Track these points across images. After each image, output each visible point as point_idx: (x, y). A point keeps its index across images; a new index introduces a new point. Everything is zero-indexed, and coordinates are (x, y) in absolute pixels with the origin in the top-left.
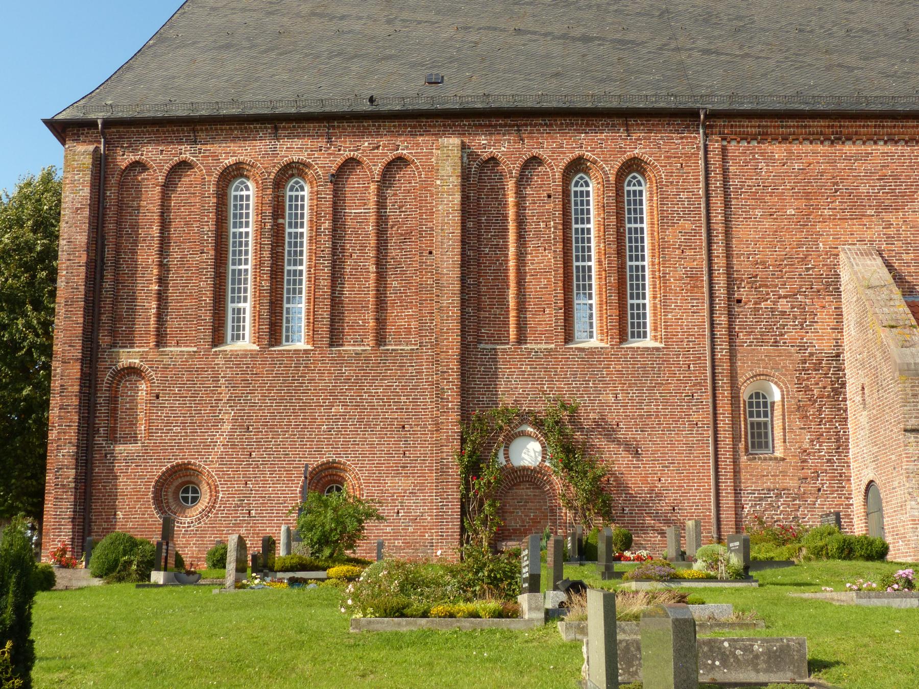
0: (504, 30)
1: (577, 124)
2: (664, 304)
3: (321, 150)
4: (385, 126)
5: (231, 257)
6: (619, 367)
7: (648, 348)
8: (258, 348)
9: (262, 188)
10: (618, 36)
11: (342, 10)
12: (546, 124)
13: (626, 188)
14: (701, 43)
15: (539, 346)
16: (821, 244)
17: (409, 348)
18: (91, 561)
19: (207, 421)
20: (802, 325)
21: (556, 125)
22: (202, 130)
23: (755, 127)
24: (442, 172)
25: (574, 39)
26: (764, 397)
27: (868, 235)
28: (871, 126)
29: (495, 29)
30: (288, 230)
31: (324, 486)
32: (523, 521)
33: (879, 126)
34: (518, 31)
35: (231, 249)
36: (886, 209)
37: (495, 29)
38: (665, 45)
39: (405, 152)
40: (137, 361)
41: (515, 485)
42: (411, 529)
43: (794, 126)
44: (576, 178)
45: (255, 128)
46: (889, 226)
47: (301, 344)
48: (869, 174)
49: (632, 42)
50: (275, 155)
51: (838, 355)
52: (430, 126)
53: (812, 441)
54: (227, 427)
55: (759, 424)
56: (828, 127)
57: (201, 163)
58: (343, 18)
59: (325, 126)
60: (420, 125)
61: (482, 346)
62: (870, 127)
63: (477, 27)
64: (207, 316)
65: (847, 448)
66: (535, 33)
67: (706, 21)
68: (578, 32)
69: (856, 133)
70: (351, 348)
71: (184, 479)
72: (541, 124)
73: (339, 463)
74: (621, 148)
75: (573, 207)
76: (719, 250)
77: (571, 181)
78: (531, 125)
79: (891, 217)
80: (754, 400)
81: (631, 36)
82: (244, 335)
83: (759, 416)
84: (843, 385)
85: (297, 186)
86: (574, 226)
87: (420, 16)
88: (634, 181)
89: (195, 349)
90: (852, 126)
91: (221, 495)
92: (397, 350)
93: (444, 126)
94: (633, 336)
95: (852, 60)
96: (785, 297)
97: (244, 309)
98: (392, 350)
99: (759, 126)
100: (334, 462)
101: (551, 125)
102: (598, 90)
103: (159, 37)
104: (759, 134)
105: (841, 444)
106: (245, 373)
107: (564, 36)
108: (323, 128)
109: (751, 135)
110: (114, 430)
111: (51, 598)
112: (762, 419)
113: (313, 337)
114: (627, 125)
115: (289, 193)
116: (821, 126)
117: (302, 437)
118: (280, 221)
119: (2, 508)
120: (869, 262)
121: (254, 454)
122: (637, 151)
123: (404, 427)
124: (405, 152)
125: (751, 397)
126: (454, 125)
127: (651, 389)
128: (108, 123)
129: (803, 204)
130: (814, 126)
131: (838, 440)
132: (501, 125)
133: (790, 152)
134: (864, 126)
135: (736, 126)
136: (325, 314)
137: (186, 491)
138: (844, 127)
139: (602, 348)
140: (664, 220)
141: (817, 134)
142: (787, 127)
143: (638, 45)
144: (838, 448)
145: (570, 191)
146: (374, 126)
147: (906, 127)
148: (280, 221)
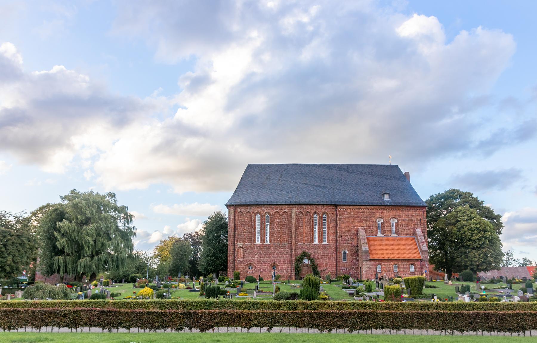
10: (323, 185)
11: (273, 178)
13: (323, 217)
14: (338, 187)
18: (437, 286)
25: (315, 186)
29: (301, 183)
36: (366, 221)
37: (301, 183)
46: (367, 224)
47: (268, 243)
49: (326, 187)
51: (357, 246)
54: (257, 257)
55: (344, 257)
58: (273, 179)
66: (308, 184)
67: (339, 181)
68: (316, 184)
81: (325, 185)
84: (358, 251)
86: (314, 223)
102: (318, 200)
107: (313, 185)
108: (272, 206)
128: (236, 205)
137: (250, 267)
143: (327, 188)
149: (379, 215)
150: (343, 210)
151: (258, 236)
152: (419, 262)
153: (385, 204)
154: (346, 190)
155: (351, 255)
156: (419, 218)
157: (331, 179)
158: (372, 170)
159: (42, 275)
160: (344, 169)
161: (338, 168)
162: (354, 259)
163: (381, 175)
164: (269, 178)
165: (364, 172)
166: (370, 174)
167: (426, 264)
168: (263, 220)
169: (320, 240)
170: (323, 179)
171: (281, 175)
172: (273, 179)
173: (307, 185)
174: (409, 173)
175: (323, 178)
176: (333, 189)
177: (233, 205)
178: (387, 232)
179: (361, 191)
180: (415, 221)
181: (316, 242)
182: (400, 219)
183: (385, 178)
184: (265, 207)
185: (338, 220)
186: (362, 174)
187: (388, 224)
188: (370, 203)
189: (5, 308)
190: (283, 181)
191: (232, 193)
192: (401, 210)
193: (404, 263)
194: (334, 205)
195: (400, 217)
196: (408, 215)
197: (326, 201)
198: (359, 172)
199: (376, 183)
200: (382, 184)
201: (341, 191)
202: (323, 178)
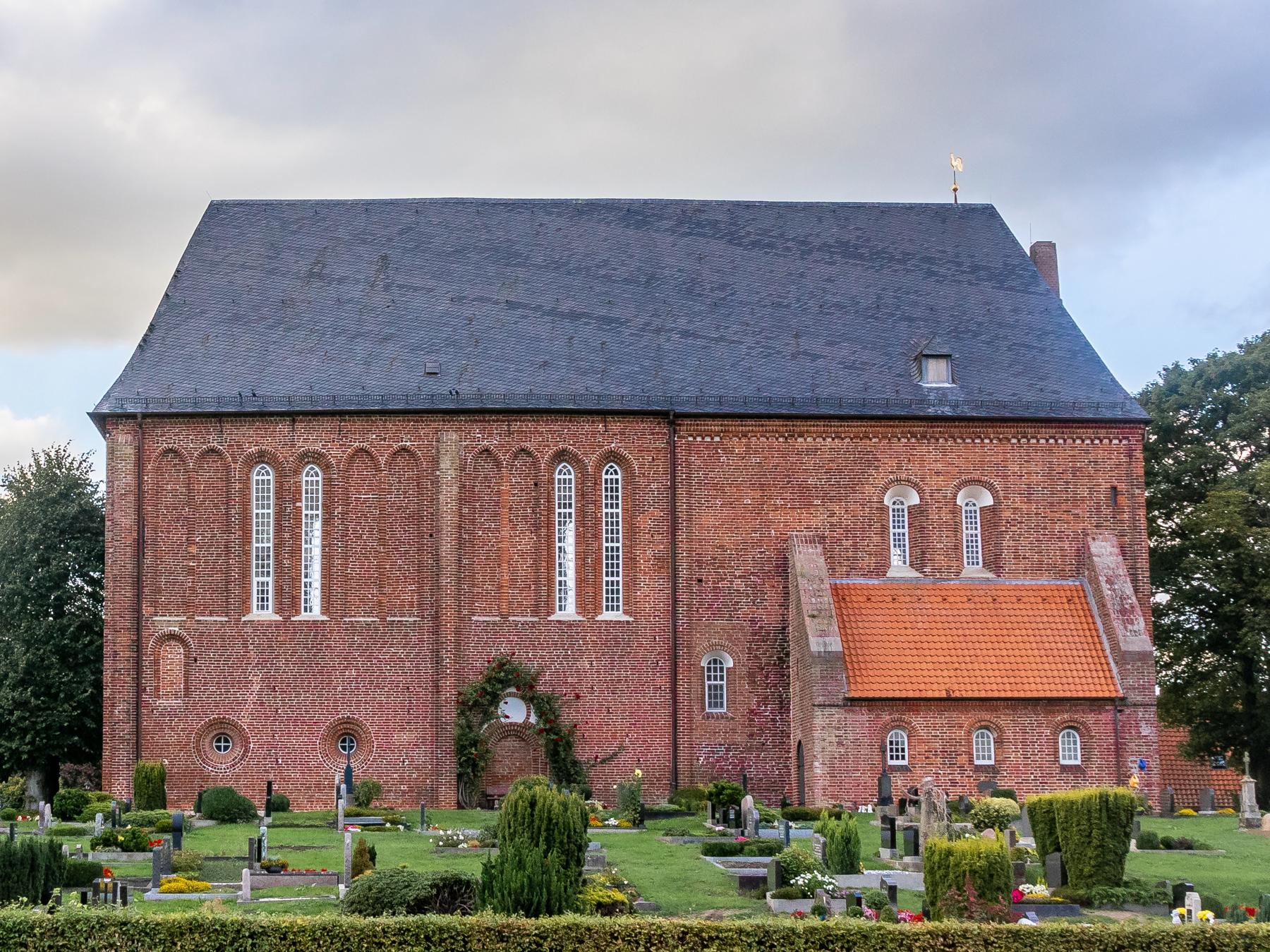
0: (497, 303)
1: (561, 420)
3: (334, 441)
4: (390, 420)
5: (254, 536)
6: (594, 638)
7: (620, 621)
8: (281, 619)
10: (603, 312)
11: (340, 272)
12: (533, 420)
14: (682, 322)
15: (525, 619)
16: (773, 532)
17: (412, 619)
18: (1202, 840)
19: (239, 682)
20: (754, 603)
21: (543, 421)
22: (227, 421)
23: (718, 426)
24: (442, 466)
25: (563, 315)
26: (721, 663)
27: (813, 523)
28: (820, 426)
30: (304, 512)
31: (339, 737)
32: (510, 769)
33: (827, 426)
34: (511, 305)
35: (255, 528)
38: (647, 324)
39: (408, 444)
40: (177, 629)
41: (503, 738)
42: (414, 776)
43: (752, 425)
44: (560, 467)
45: (275, 420)
47: (316, 613)
48: (818, 468)
49: (616, 320)
50: (293, 446)
51: (784, 629)
52: (431, 421)
53: (758, 703)
54: (256, 687)
55: (716, 686)
56: (783, 426)
57: (228, 452)
59: (337, 420)
60: (422, 420)
61: (474, 618)
62: (820, 426)
63: (471, 297)
65: (788, 710)
66: (525, 306)
67: (690, 291)
68: (565, 307)
69: (807, 431)
70: (362, 619)
71: (222, 731)
72: (529, 420)
73: (353, 718)
74: (599, 442)
75: (557, 493)
77: (554, 470)
78: (520, 421)
80: (712, 666)
81: (616, 313)
82: (267, 605)
83: (715, 679)
84: (788, 655)
85: (312, 472)
87: (417, 282)
88: (612, 470)
89: (226, 619)
90: (803, 426)
91: (252, 746)
92: (402, 621)
93: (444, 421)
94: (607, 609)
95: (817, 346)
96: (740, 577)
97: (267, 583)
98: (398, 621)
99: (721, 425)
100: (348, 717)
101: (538, 421)
104: (722, 432)
105: (783, 707)
106: (270, 640)
107: (552, 312)
108: (337, 422)
109: (715, 432)
110: (157, 689)
112: (719, 682)
113: (326, 610)
114: (605, 422)
115: (305, 479)
116: (776, 426)
117: (321, 696)
118: (298, 504)
120: (811, 550)
121: (280, 711)
122: (613, 445)
123: (408, 688)
124: (408, 444)
125: (709, 663)
126: (452, 420)
127: (621, 656)
128: (145, 416)
129: (758, 494)
130: (769, 426)
131: (781, 702)
132: (494, 421)
133: (748, 446)
134: (814, 426)
135: (701, 425)
138: (796, 426)
139: (579, 621)
141: (773, 432)
142: (745, 426)
143: (622, 324)
144: (781, 709)
145: (554, 479)
146: (381, 420)
147: (851, 426)
148: (298, 504)
149: (900, 468)
150: (708, 439)
151: (262, 580)
153: (931, 411)
154: (722, 339)
155: (751, 675)
156: (1105, 486)
157: (643, 279)
158: (859, 233)
162: (764, 701)
164: (320, 276)
165: (817, 242)
166: (848, 251)
167: (1143, 724)
168: (287, 496)
170: (604, 276)
171: (385, 258)
172: (341, 281)
173: (520, 311)
174: (1052, 246)
175: (602, 272)
176: (658, 331)
177: (133, 416)
178: (941, 560)
179: (804, 343)
180: (1083, 500)
181: (263, 614)
182: (1006, 489)
183: (931, 273)
184: (298, 425)
186: (810, 252)
187: (946, 517)
190: (395, 290)
191: (127, 349)
192: (1014, 441)
193: (1027, 719)
194: (661, 415)
195: (1005, 476)
196: (1051, 469)
197: (620, 392)
198: (790, 244)
199: (879, 297)
201: (700, 342)
202: (602, 272)
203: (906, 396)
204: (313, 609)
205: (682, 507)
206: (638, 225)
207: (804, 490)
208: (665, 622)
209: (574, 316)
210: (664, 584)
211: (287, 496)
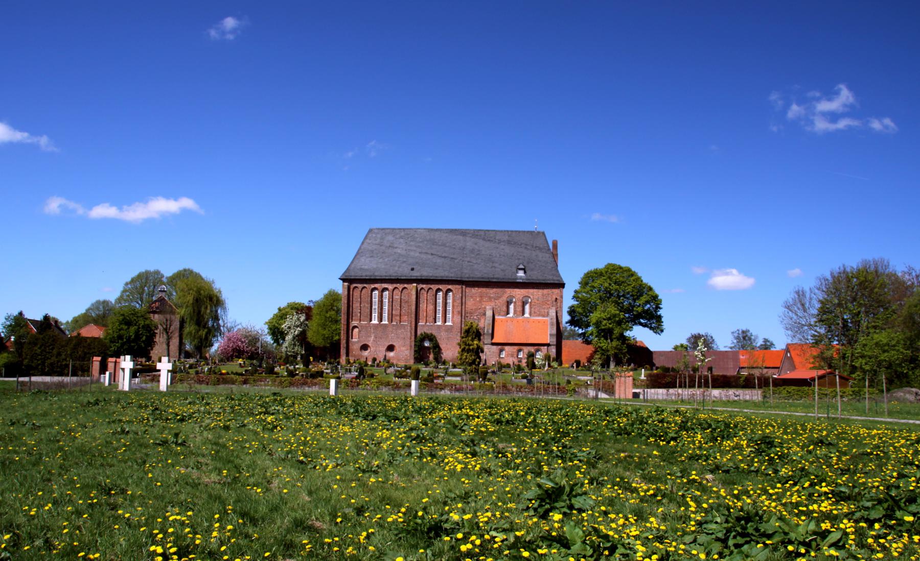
2: (453, 317)
9: (379, 292)
47: (386, 322)
64: (369, 317)
68: (443, 255)
76: (463, 307)
79: (496, 301)
103: (358, 254)
111: (880, 295)
119: (919, 515)
136: (390, 317)
140: (454, 301)
151: (375, 315)
152: (546, 347)
154: (476, 263)
156: (554, 297)
159: (506, 362)
160: (480, 236)
161: (473, 235)
163: (522, 244)
164: (392, 247)
168: (381, 297)
169: (381, 319)
172: (396, 248)
179: (494, 265)
181: (375, 321)
185: (464, 298)
188: (520, 279)
189: (300, 390)
195: (533, 295)
200: (520, 256)
203: (513, 277)
204: (385, 322)
205: (464, 301)
206: (463, 235)
207: (490, 298)
208: (460, 325)
209: (445, 257)
210: (460, 317)
211: (381, 297)
